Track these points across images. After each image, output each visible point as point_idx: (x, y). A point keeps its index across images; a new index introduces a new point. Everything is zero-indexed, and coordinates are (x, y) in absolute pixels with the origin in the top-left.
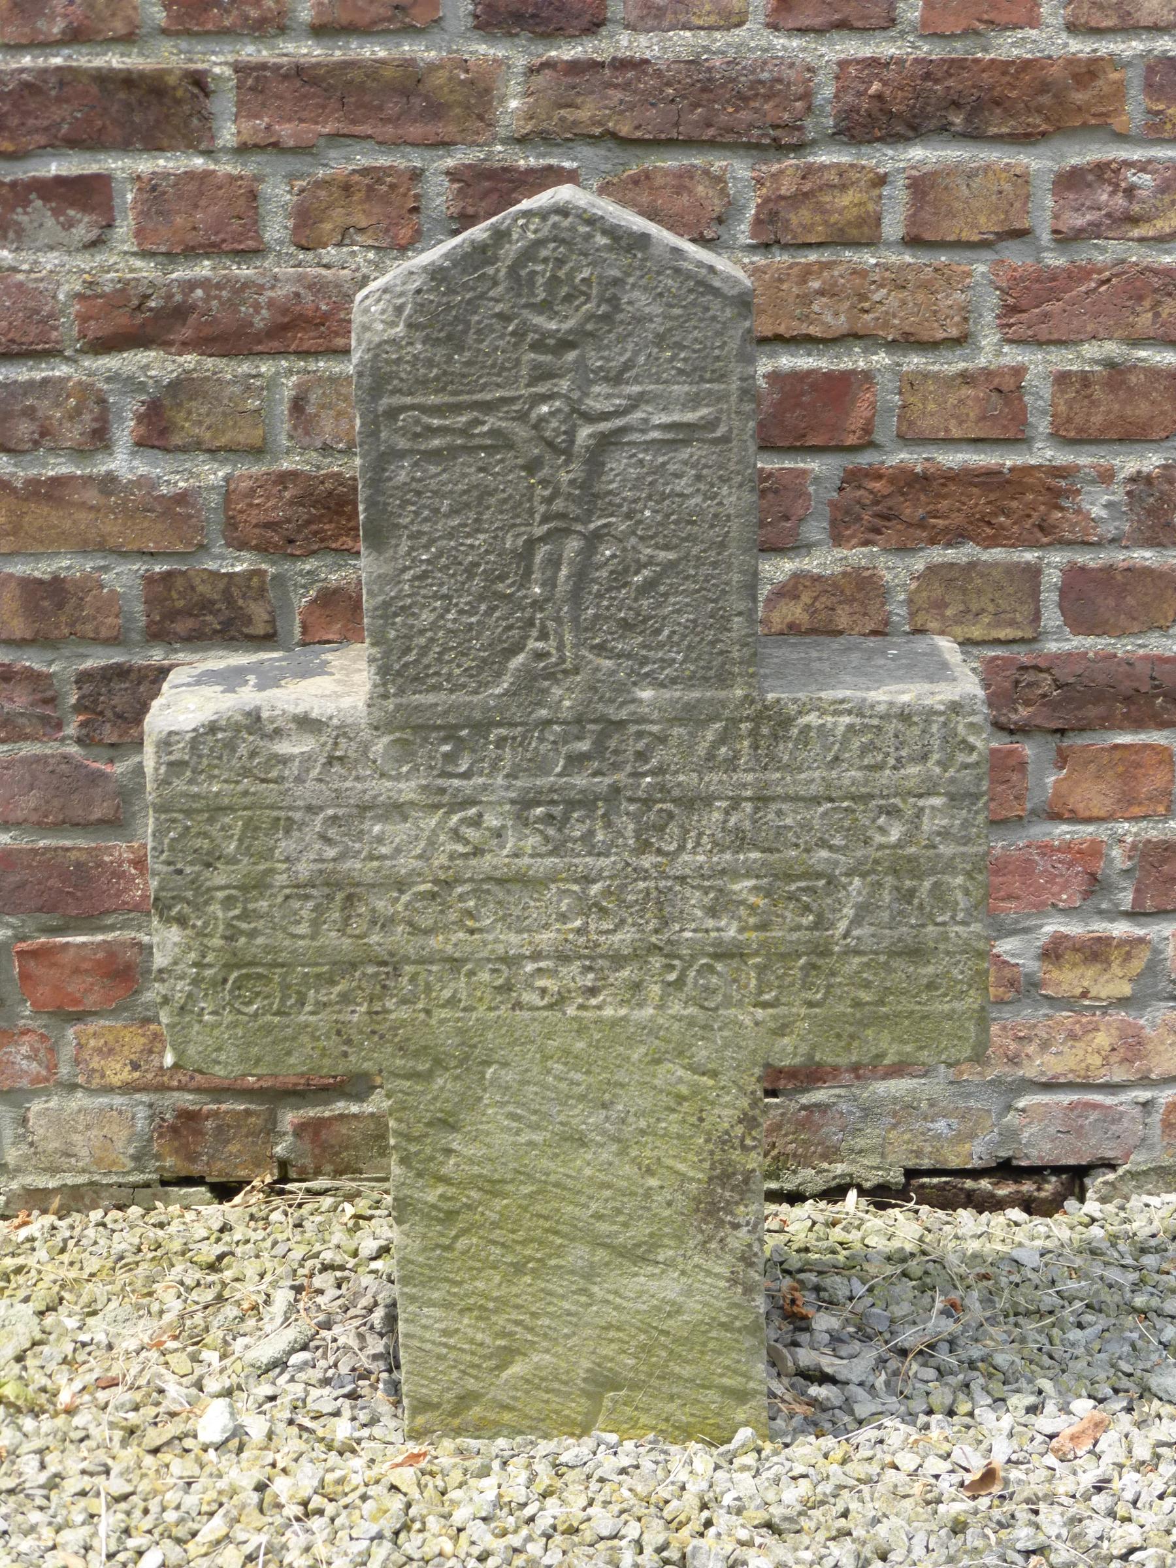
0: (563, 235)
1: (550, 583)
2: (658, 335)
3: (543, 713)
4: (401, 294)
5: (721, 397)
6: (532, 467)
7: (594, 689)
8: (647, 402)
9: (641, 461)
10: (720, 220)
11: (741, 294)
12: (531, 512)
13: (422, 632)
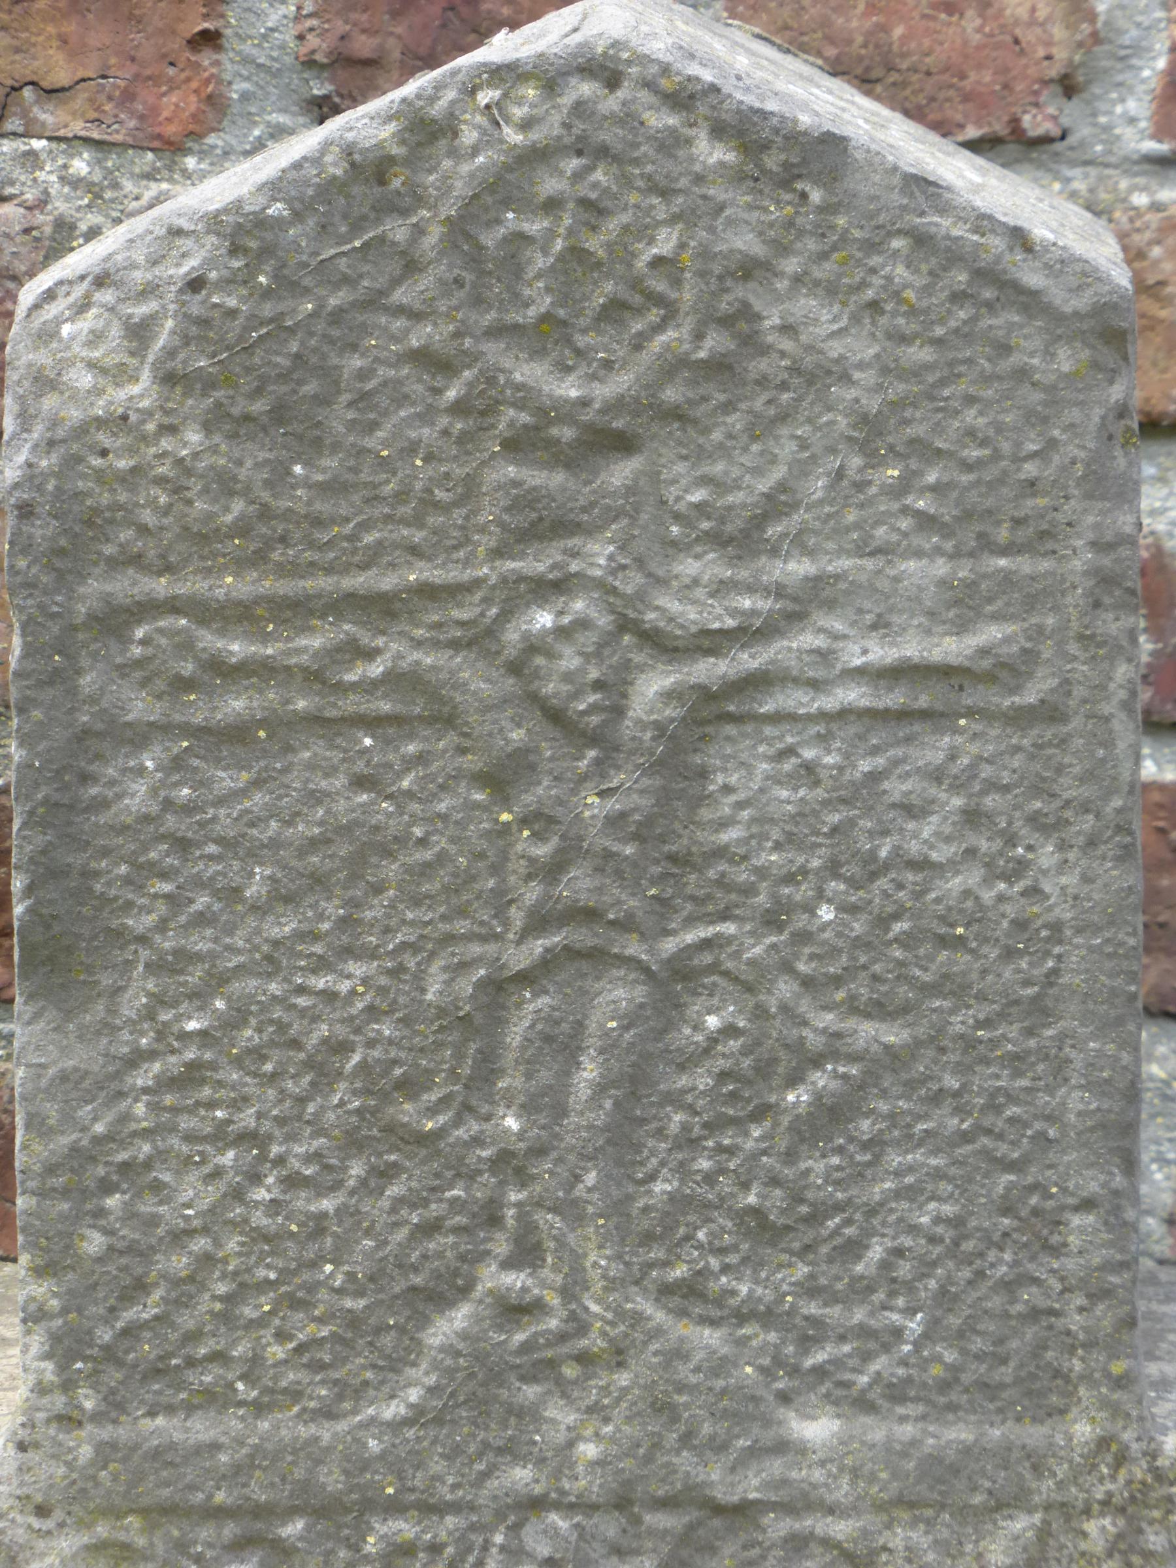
0: (605, 136)
1: (546, 1105)
2: (864, 420)
3: (521, 1475)
4: (149, 291)
5: (1034, 597)
6: (500, 779)
7: (664, 1409)
8: (830, 605)
9: (809, 768)
10: (1068, 87)
11: (1099, 310)
12: (501, 902)
13: (179, 1237)
